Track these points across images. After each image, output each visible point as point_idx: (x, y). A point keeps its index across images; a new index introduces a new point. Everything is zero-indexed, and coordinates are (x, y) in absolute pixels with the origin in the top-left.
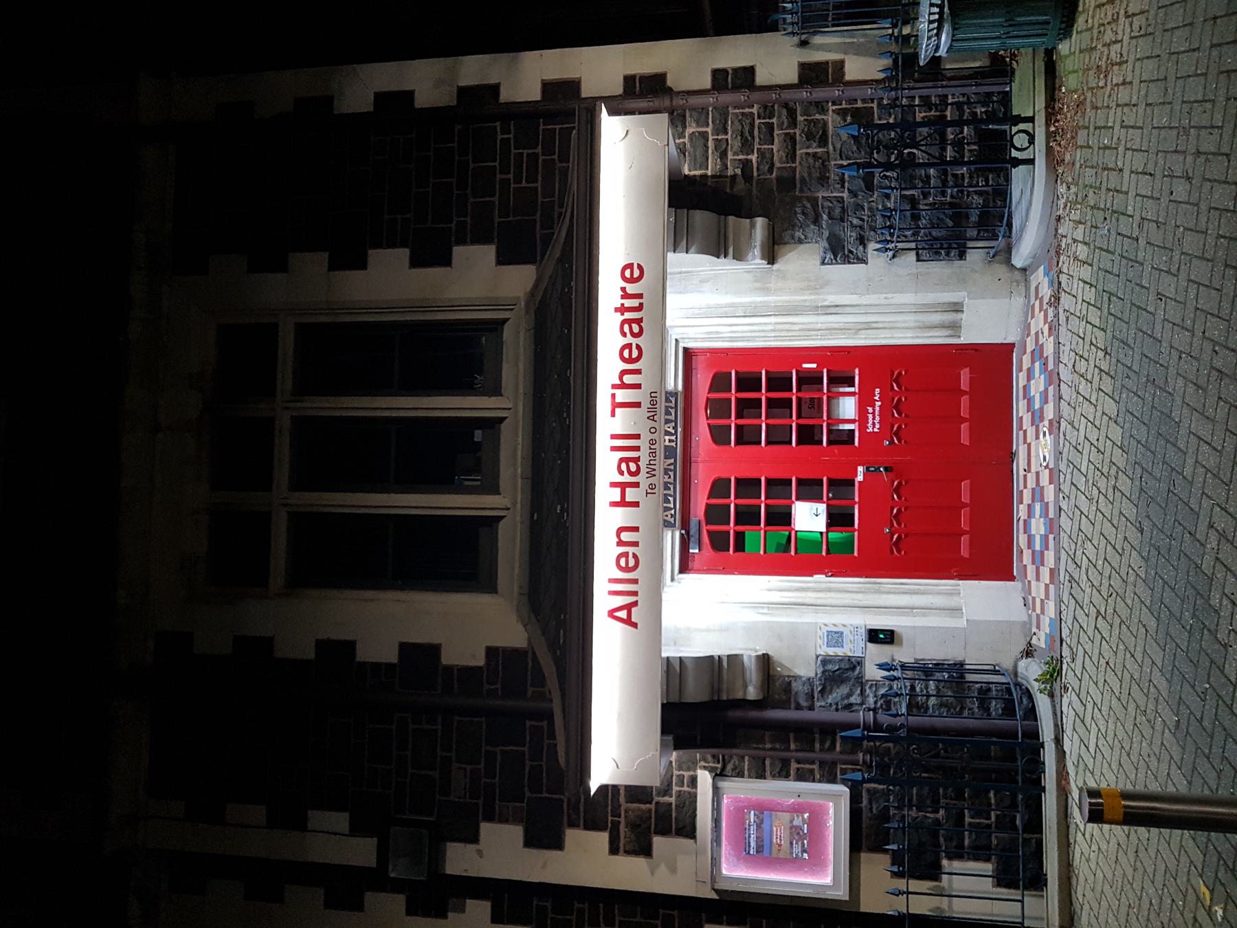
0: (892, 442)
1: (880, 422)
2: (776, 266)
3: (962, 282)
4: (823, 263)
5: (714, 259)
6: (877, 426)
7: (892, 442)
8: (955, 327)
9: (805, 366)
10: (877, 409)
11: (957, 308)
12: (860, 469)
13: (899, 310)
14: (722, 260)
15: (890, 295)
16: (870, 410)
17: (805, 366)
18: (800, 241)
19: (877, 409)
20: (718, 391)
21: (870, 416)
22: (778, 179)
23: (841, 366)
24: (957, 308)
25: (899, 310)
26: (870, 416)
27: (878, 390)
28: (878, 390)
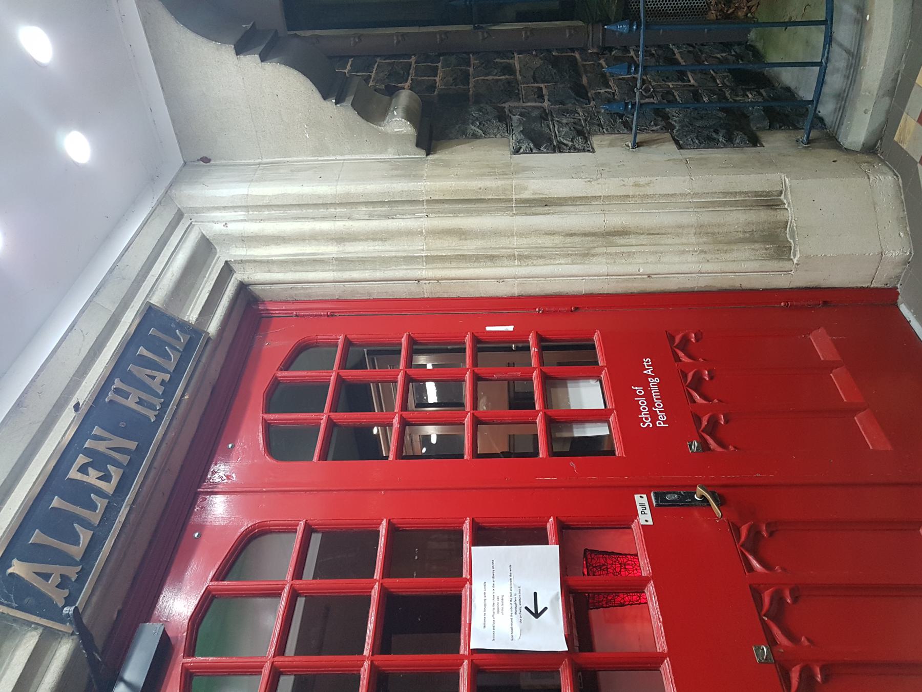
0: (704, 446)
1: (666, 410)
2: (431, 157)
3: (770, 164)
4: (517, 151)
5: (317, 95)
6: (662, 417)
7: (704, 446)
8: (776, 242)
9: (488, 329)
10: (655, 390)
11: (770, 201)
12: (641, 500)
13: (667, 200)
14: (330, 104)
15: (642, 180)
16: (639, 390)
17: (488, 329)
18: (475, 136)
19: (655, 390)
20: (319, 651)
21: (643, 403)
22: (439, 95)
23: (567, 332)
24: (770, 201)
25: (667, 200)
26: (643, 403)
27: (647, 362)
28: (647, 362)
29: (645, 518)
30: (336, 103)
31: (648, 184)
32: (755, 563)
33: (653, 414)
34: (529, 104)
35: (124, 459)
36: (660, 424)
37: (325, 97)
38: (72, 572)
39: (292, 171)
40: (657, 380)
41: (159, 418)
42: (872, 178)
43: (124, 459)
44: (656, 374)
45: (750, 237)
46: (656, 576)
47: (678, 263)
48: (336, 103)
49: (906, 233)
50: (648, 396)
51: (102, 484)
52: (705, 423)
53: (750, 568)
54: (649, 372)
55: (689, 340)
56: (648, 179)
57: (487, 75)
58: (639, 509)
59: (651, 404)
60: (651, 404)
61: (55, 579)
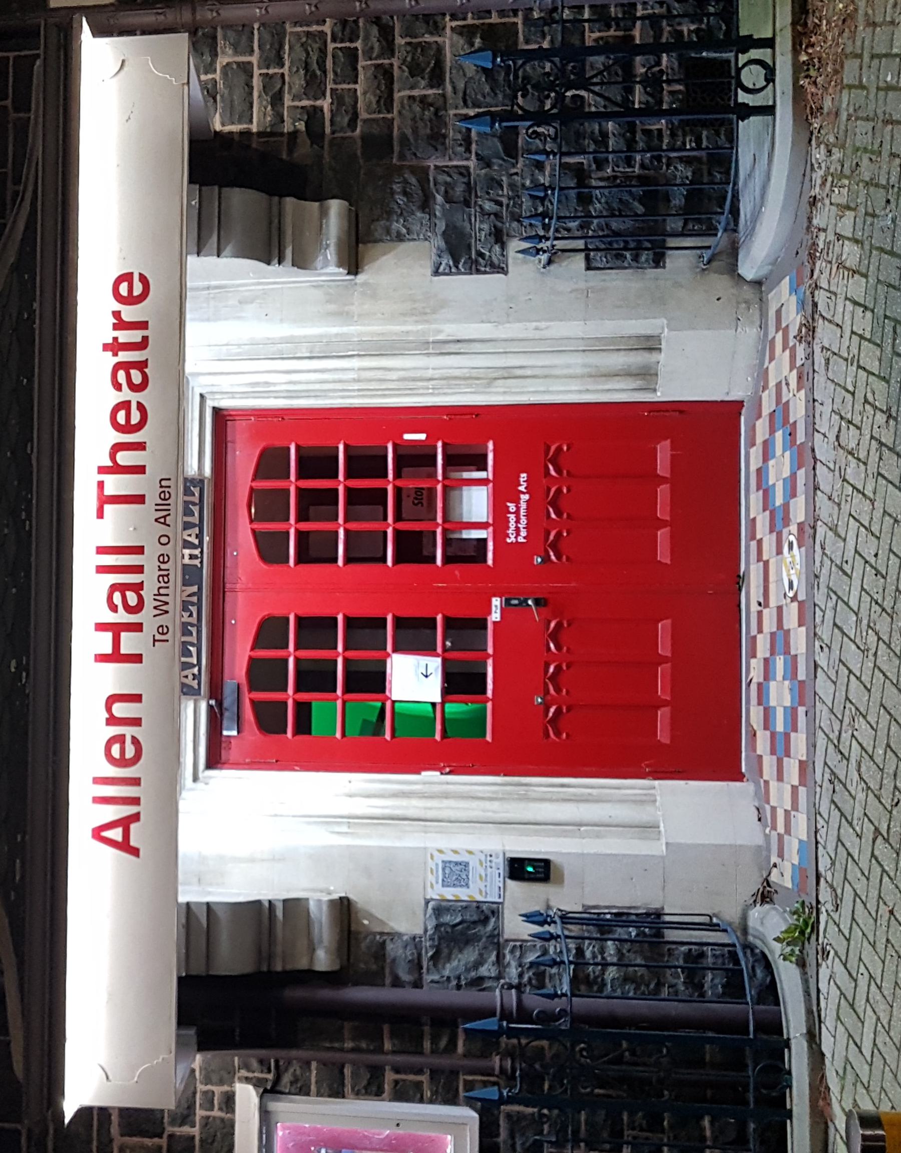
0: (546, 559)
2: (361, 278)
4: (436, 273)
5: (262, 265)
6: (523, 533)
7: (546, 559)
9: (407, 437)
10: (523, 512)
11: (651, 344)
12: (496, 602)
14: (275, 268)
15: (543, 324)
16: (512, 507)
17: (407, 437)
18: (400, 238)
21: (512, 517)
22: (364, 138)
26: (512, 517)
27: (524, 476)
28: (524, 476)
29: (496, 616)
30: (279, 264)
31: (547, 328)
32: (552, 645)
33: (517, 531)
34: (455, 163)
35: (195, 599)
36: (521, 540)
37: (269, 263)
38: (196, 670)
39: (240, 302)
40: (527, 497)
41: (201, 562)
42: (739, 329)
43: (195, 599)
44: (529, 490)
45: (628, 373)
46: (494, 656)
47: (565, 383)
48: (279, 264)
49: (753, 378)
50: (517, 513)
51: (190, 620)
52: (551, 537)
53: (549, 649)
54: (522, 488)
55: (562, 449)
56: (548, 324)
57: (412, 88)
58: (494, 609)
59: (518, 521)
60: (518, 521)
61: (191, 677)
